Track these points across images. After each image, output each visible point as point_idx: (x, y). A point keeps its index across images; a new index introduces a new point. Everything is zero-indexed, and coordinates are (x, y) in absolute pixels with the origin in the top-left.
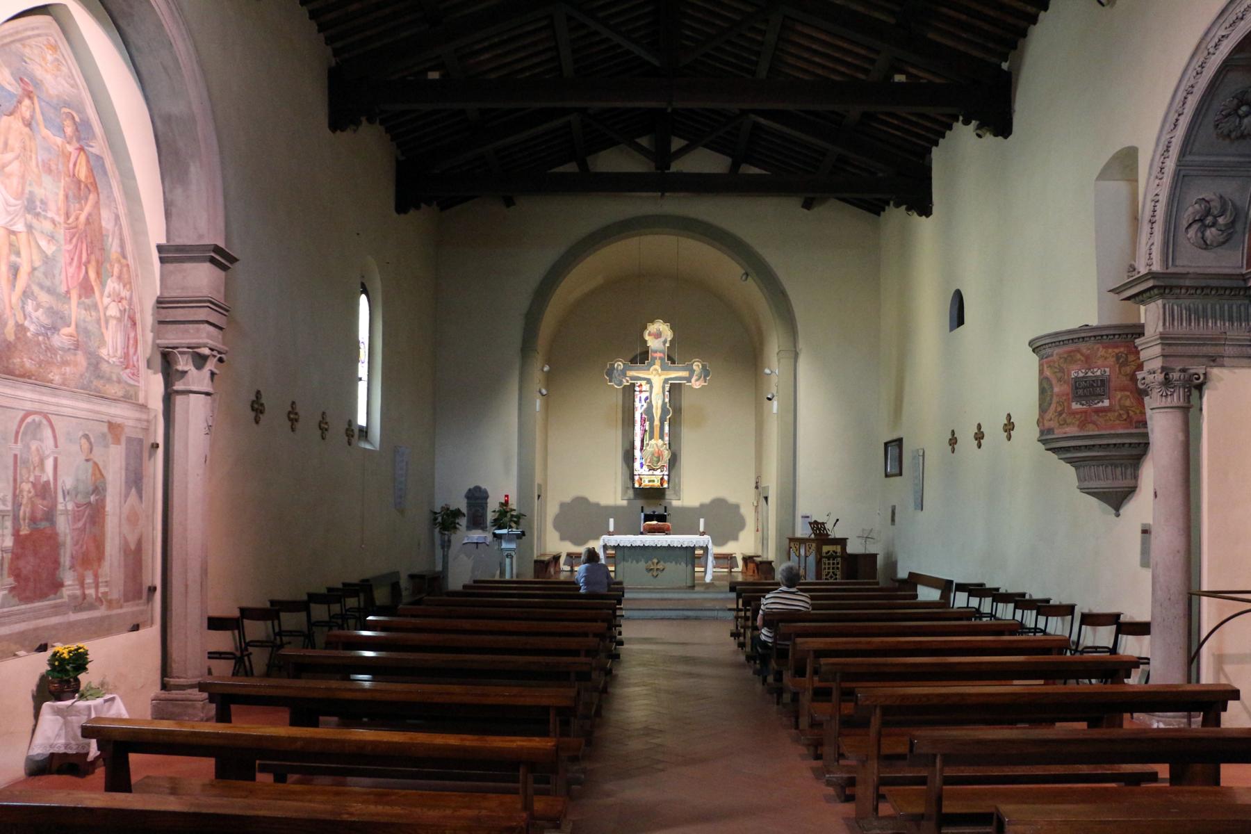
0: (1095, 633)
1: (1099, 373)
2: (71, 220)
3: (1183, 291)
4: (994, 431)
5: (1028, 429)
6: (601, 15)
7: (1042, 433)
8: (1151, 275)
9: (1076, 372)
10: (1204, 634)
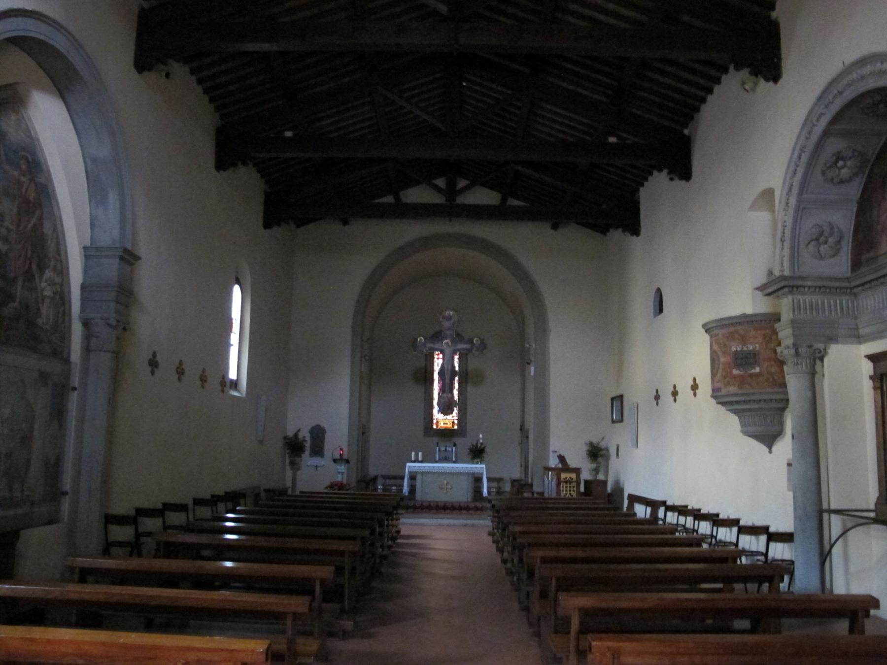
1: (751, 348)
2: (21, 228)
3: (806, 289)
4: (684, 389)
5: (705, 387)
6: (406, 95)
7: (713, 390)
8: (783, 278)
9: (735, 347)
10: (833, 540)
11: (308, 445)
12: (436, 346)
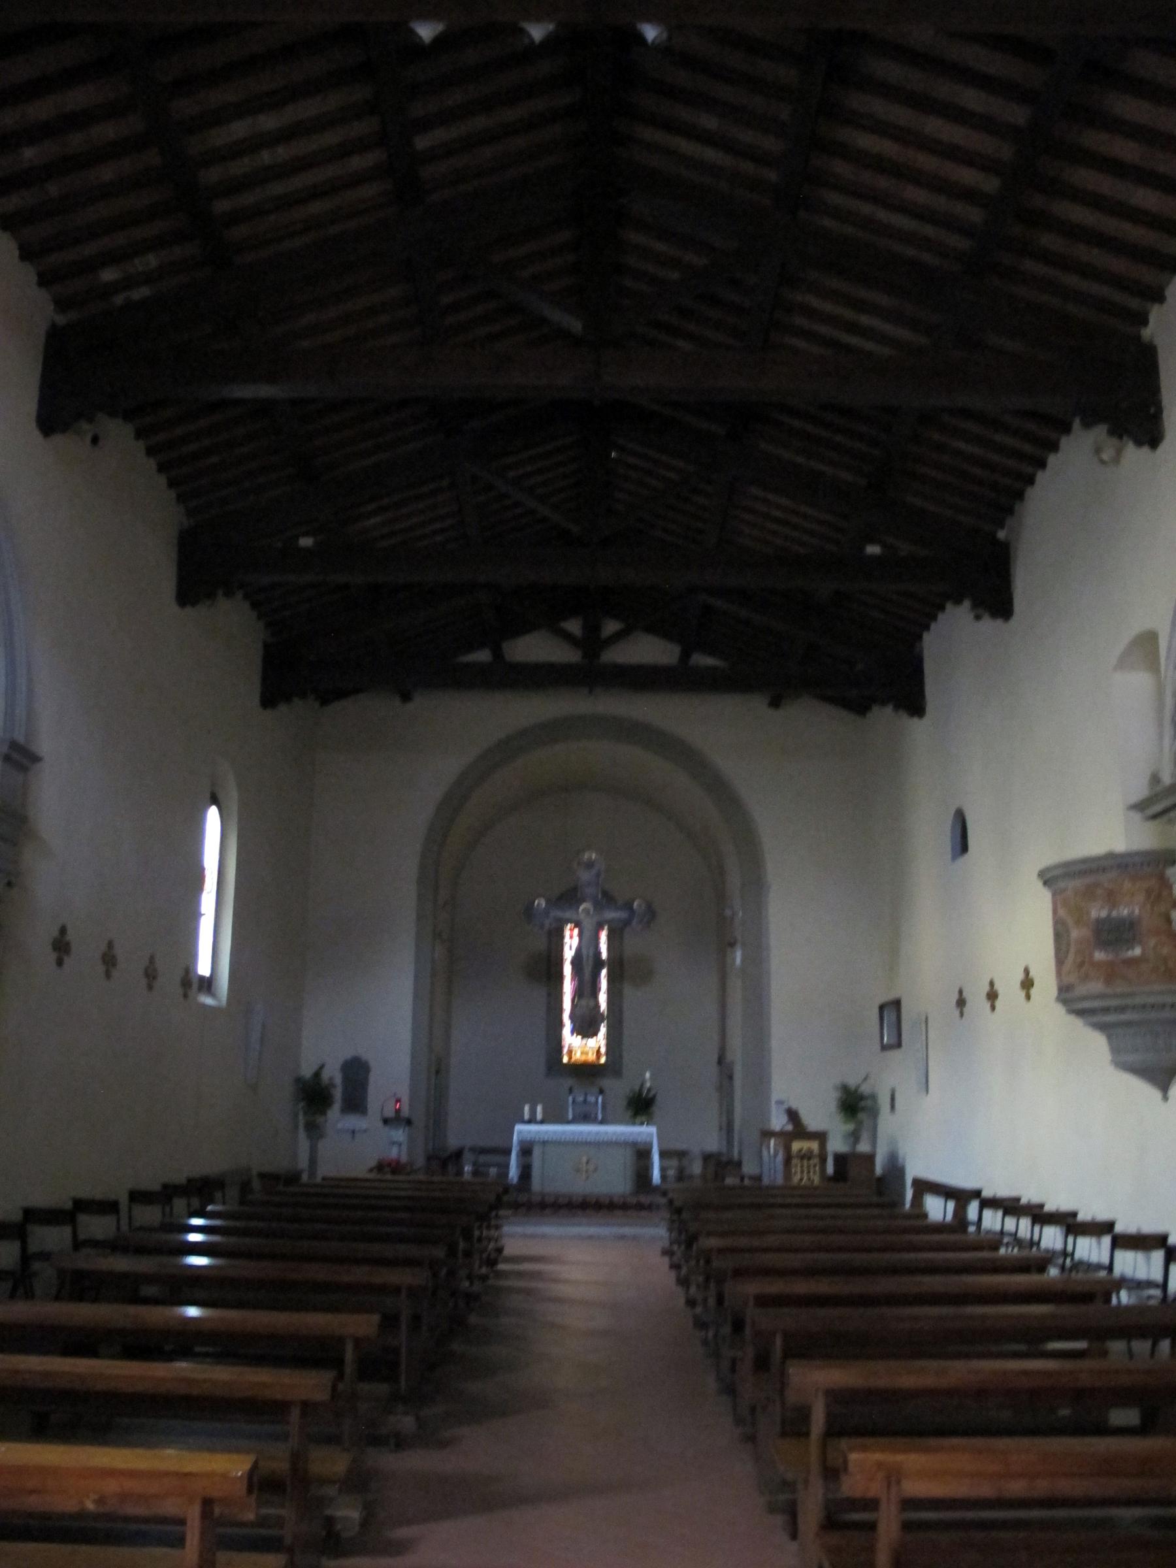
0: (1148, 1259)
9: (1098, 912)
11: (338, 1094)
12: (568, 915)
